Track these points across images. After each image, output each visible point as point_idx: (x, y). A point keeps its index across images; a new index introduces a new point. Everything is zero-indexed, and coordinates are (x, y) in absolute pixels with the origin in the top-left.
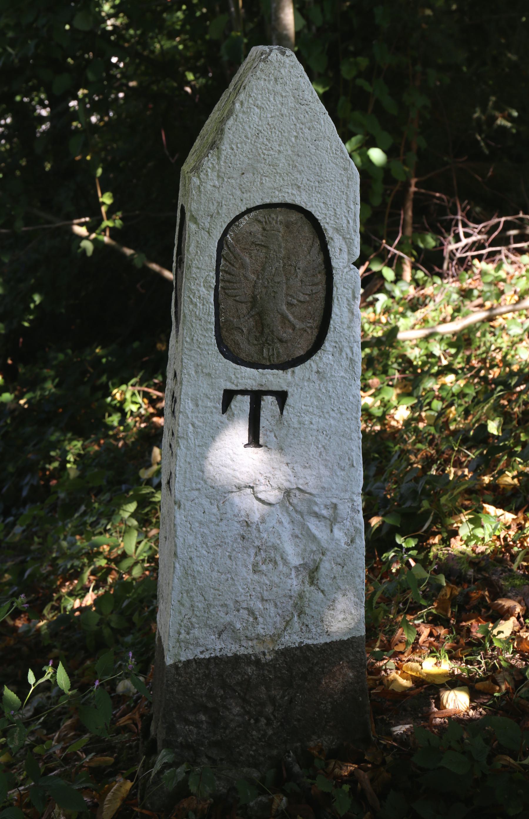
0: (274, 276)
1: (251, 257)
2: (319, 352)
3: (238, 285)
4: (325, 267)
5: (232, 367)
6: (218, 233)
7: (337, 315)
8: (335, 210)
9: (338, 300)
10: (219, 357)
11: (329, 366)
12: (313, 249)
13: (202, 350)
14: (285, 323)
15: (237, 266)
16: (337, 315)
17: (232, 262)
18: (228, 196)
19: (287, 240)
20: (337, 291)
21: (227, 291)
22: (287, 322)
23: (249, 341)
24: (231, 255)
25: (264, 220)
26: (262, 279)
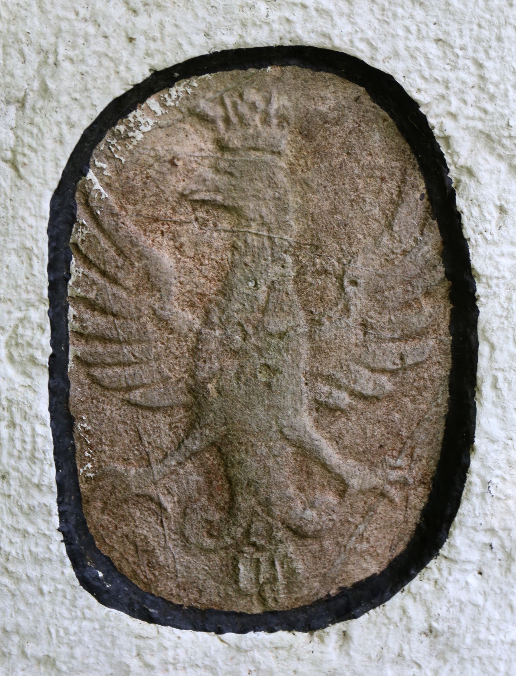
0: (264, 311)
1: (180, 248)
2: (432, 564)
3: (137, 349)
4: (448, 275)
5: (130, 634)
6: (50, 166)
7: (493, 441)
8: (480, 66)
9: (495, 386)
10: (81, 602)
11: (469, 610)
12: (403, 211)
13: (18, 580)
14: (310, 474)
15: (129, 283)
16: (493, 441)
17: (110, 269)
18: (80, 26)
19: (306, 182)
20: (491, 358)
21: (97, 372)
22: (316, 469)
23: (186, 539)
24: (104, 243)
25: (220, 111)
26: (223, 326)
